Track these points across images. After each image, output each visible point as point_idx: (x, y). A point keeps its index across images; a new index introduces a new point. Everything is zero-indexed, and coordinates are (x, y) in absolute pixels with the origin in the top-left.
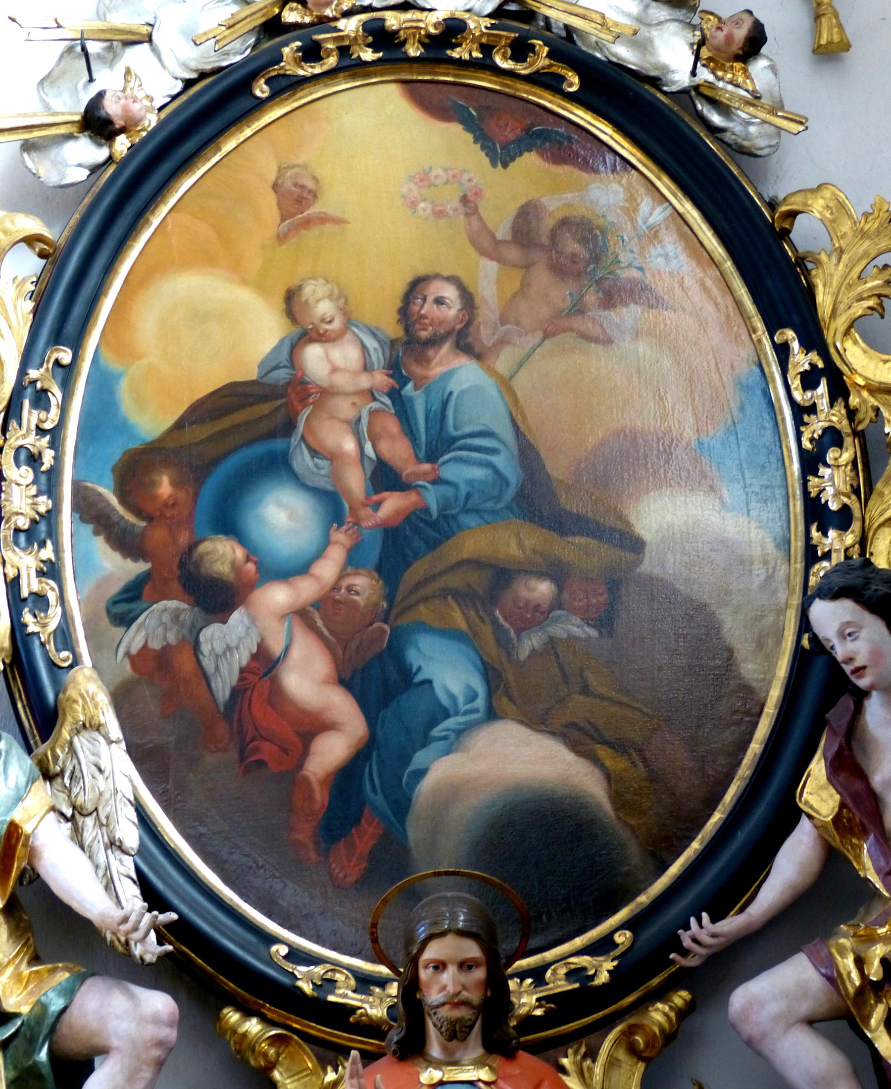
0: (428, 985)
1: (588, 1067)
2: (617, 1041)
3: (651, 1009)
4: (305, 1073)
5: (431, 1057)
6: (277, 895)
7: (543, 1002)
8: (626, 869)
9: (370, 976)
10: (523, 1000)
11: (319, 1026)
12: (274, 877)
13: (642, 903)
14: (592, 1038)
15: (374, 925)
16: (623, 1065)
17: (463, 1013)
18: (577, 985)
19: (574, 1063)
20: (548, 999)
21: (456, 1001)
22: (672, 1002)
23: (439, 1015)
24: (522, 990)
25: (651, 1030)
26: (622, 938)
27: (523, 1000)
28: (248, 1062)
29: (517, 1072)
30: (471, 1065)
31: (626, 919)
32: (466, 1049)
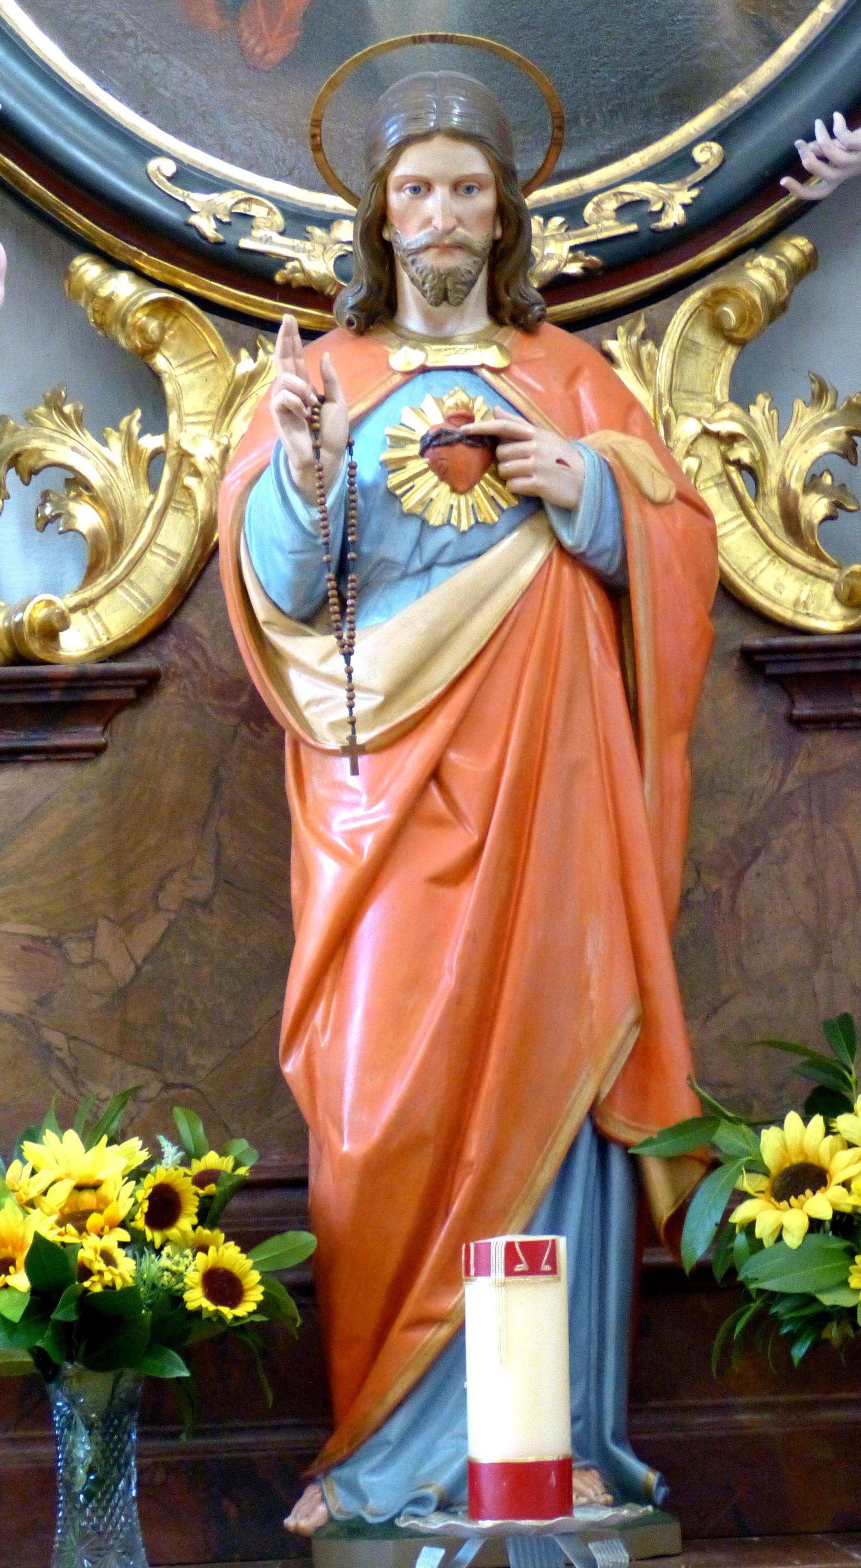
0: (403, 218)
1: (649, 354)
2: (695, 315)
3: (748, 265)
4: (205, 360)
5: (409, 331)
6: (156, 80)
7: (580, 252)
8: (713, 45)
9: (308, 210)
10: (548, 250)
11: (225, 288)
12: (149, 50)
13: (737, 100)
14: (654, 310)
15: (317, 123)
16: (704, 351)
17: (459, 261)
18: (633, 227)
19: (627, 347)
20: (588, 247)
21: (447, 241)
22: (782, 255)
23: (420, 265)
24: (547, 234)
25: (749, 297)
26: (701, 154)
27: (548, 250)
28: (115, 343)
29: (541, 354)
30: (471, 342)
31: (713, 124)
32: (462, 317)
